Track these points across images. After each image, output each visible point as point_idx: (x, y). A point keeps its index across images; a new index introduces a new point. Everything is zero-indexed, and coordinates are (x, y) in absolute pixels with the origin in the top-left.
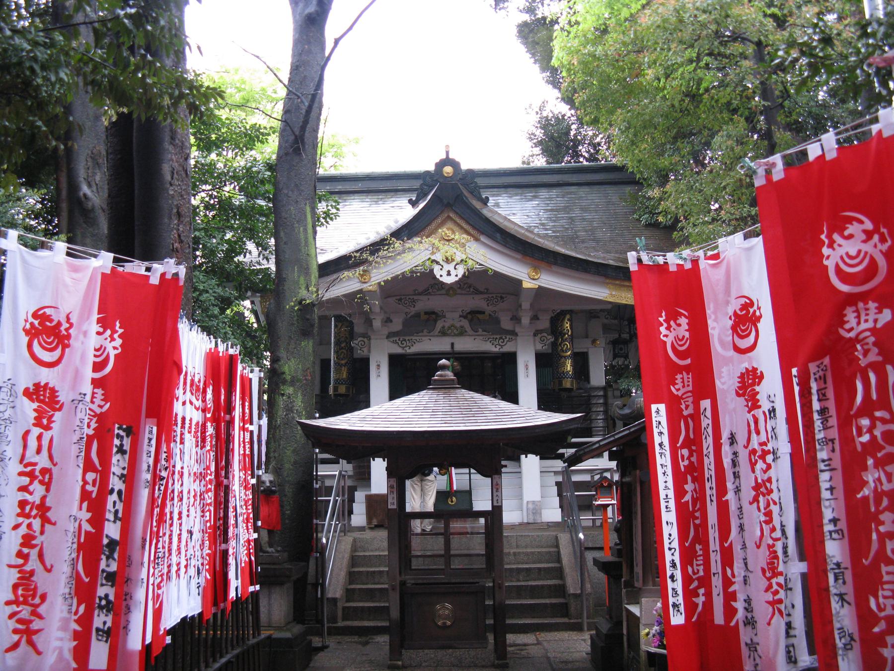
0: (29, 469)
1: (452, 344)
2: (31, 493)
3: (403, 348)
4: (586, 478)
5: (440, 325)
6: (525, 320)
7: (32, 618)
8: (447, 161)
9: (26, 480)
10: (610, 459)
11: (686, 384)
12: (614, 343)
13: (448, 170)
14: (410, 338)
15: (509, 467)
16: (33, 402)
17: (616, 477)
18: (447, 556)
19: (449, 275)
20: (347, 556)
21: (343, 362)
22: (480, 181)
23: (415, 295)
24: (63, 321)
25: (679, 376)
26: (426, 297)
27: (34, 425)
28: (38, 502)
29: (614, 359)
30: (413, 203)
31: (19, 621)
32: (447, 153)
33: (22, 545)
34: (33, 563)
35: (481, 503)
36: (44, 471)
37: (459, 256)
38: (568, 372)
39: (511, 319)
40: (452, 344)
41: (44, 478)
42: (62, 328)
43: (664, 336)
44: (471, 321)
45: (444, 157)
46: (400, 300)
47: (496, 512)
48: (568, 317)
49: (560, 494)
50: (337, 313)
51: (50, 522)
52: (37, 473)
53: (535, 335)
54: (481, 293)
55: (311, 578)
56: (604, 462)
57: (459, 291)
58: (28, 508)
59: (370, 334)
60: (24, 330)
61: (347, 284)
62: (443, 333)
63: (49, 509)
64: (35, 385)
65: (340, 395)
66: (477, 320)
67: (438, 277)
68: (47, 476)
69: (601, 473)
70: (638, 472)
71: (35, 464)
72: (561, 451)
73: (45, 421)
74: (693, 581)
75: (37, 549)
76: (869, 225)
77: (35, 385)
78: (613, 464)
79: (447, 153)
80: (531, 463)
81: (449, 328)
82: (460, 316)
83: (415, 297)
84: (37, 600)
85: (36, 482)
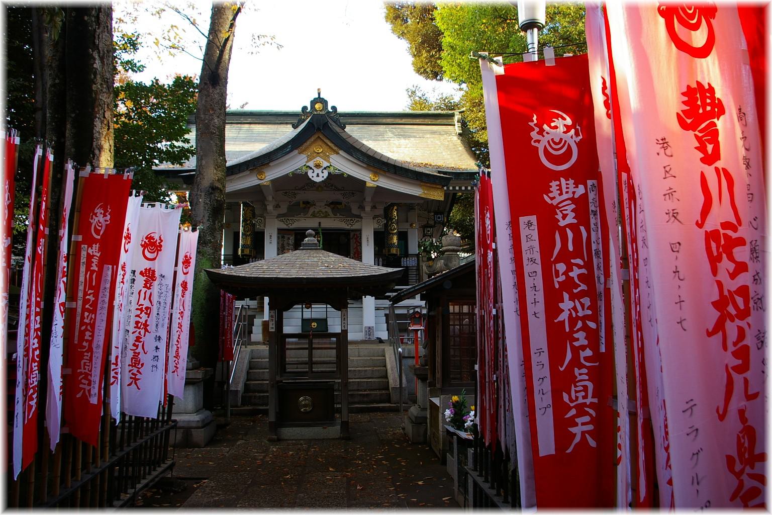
0: (141, 307)
1: (320, 223)
2: (141, 318)
3: (287, 225)
4: (404, 311)
5: (311, 210)
6: (368, 209)
7: (137, 373)
8: (319, 100)
9: (139, 312)
10: (421, 300)
11: (564, 190)
12: (424, 227)
13: (318, 106)
14: (292, 218)
15: (352, 305)
16: (144, 277)
17: (424, 312)
18: (311, 363)
19: (318, 176)
20: (246, 361)
21: (248, 233)
22: (342, 120)
23: (296, 190)
24: (158, 239)
25: (554, 184)
26: (304, 191)
27: (143, 287)
28: (144, 322)
29: (424, 237)
30: (295, 127)
31: (133, 374)
32: (319, 94)
33: (135, 341)
34: (140, 350)
35: (335, 326)
36: (147, 308)
37: (325, 164)
38: (394, 243)
39: (359, 208)
40: (320, 223)
41: (147, 311)
42: (157, 242)
43: (535, 141)
44: (333, 209)
45: (317, 96)
46: (286, 193)
47: (345, 332)
48: (395, 208)
49: (387, 322)
50: (244, 201)
51: (148, 332)
52: (144, 309)
53: (373, 219)
54: (339, 190)
55: (218, 378)
56: (417, 301)
57: (325, 188)
58: (139, 325)
59: (265, 215)
60: (141, 245)
61: (249, 181)
62: (314, 215)
63: (148, 325)
64: (145, 269)
65: (246, 255)
66: (336, 207)
67: (311, 177)
68: (149, 311)
69: (414, 309)
70: (440, 308)
71: (143, 305)
72: (387, 294)
73: (148, 285)
74: (570, 408)
75: (142, 343)
76: (569, 121)
77: (145, 269)
78: (423, 303)
79: (319, 94)
80: (369, 302)
81: (318, 212)
82: (326, 205)
83: (296, 192)
84: (140, 366)
85: (143, 313)
